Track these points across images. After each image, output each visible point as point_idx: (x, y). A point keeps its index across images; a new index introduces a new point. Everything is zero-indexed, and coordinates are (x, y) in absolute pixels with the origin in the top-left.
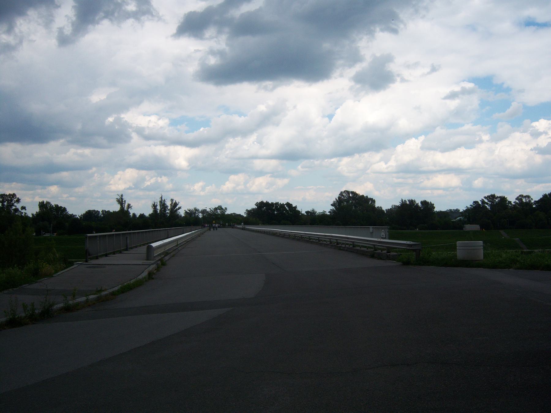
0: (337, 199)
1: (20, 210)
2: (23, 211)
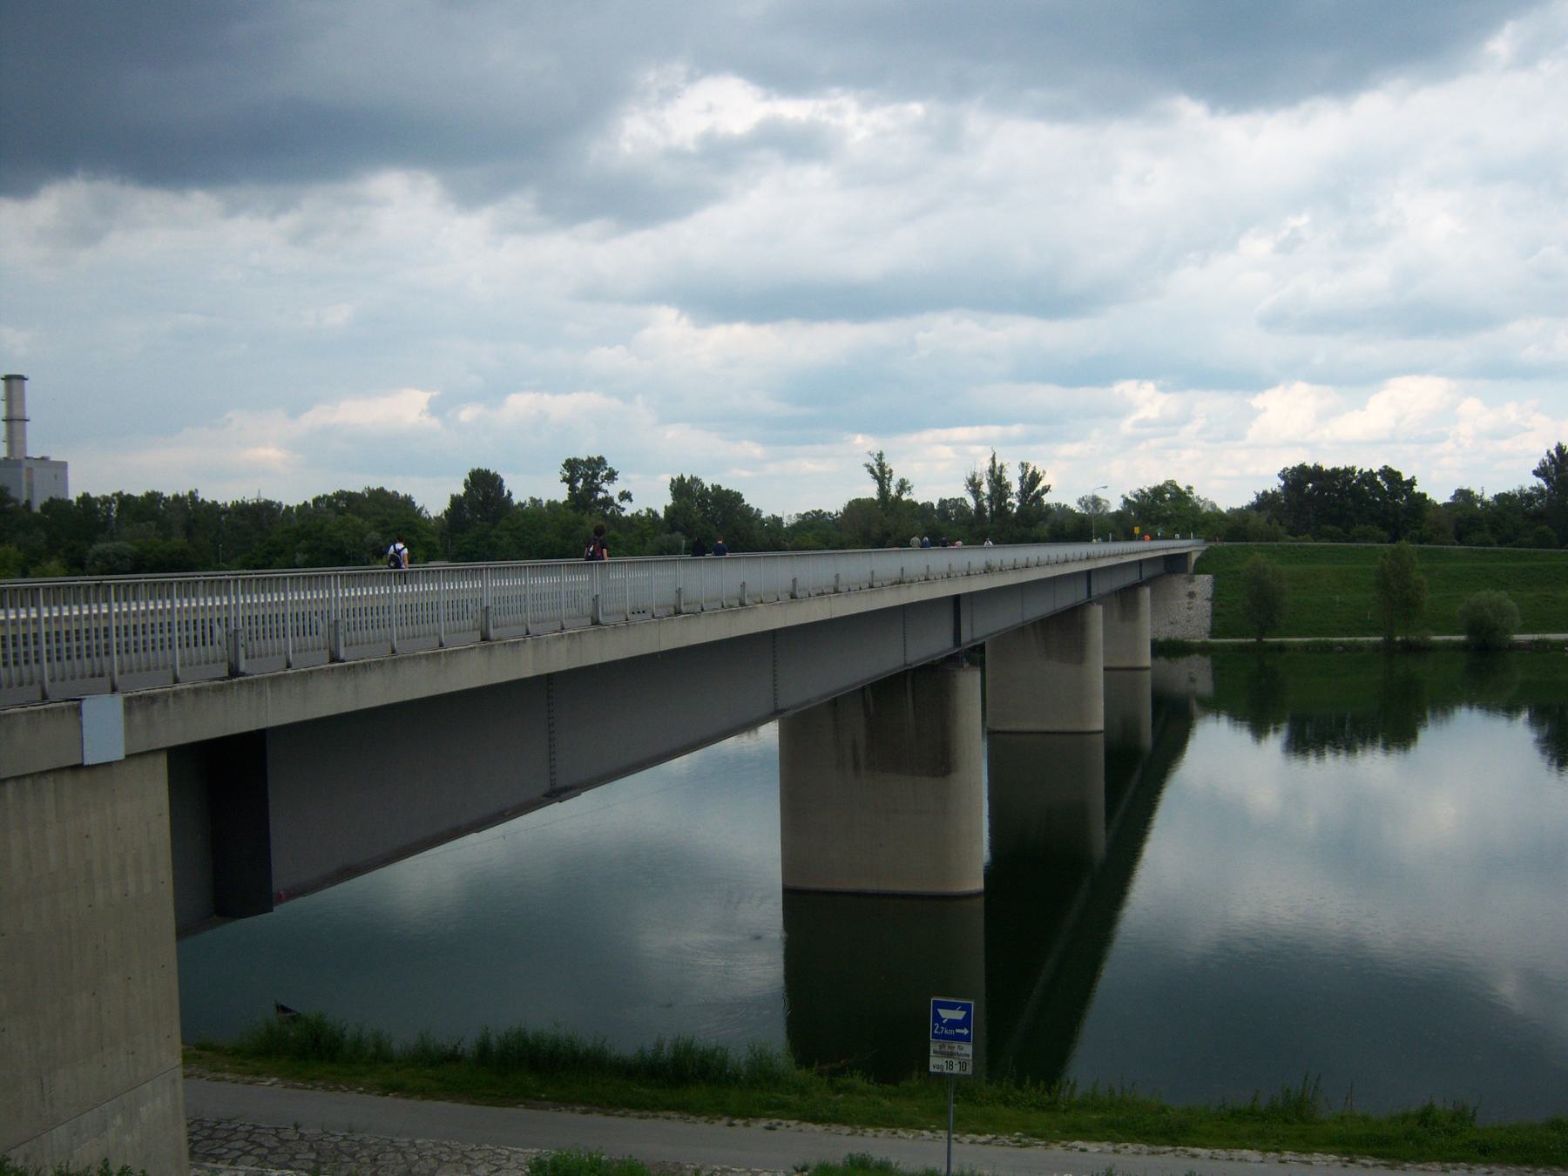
0: (1554, 452)
1: (616, 500)
2: (625, 504)
